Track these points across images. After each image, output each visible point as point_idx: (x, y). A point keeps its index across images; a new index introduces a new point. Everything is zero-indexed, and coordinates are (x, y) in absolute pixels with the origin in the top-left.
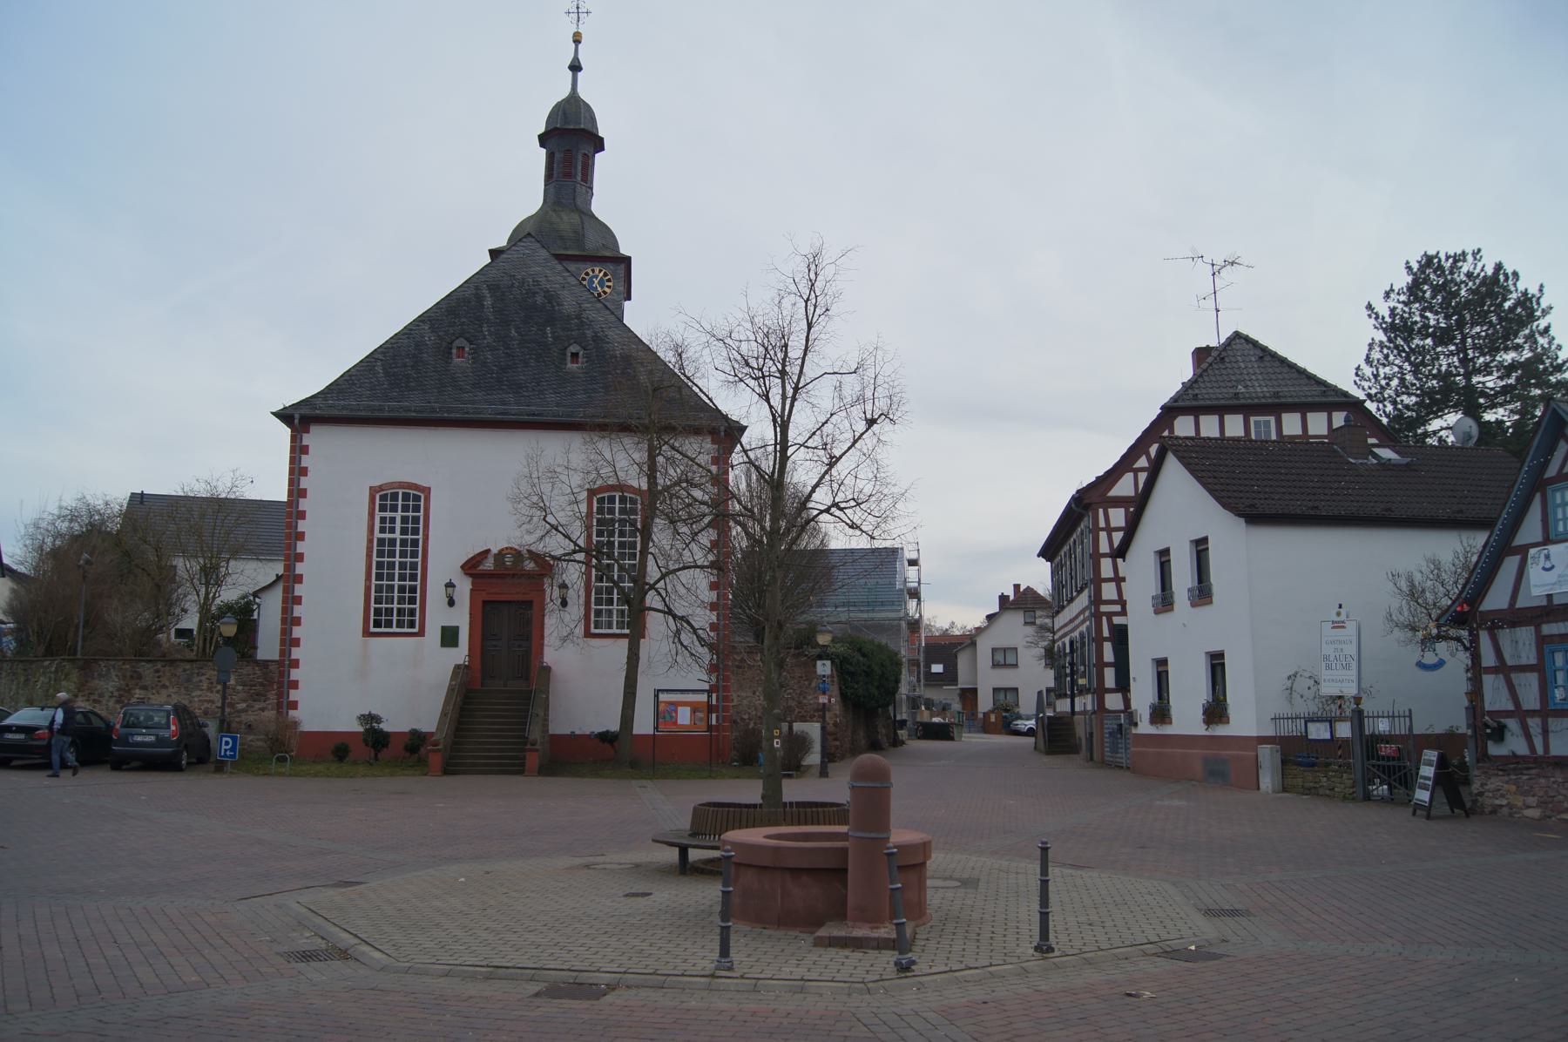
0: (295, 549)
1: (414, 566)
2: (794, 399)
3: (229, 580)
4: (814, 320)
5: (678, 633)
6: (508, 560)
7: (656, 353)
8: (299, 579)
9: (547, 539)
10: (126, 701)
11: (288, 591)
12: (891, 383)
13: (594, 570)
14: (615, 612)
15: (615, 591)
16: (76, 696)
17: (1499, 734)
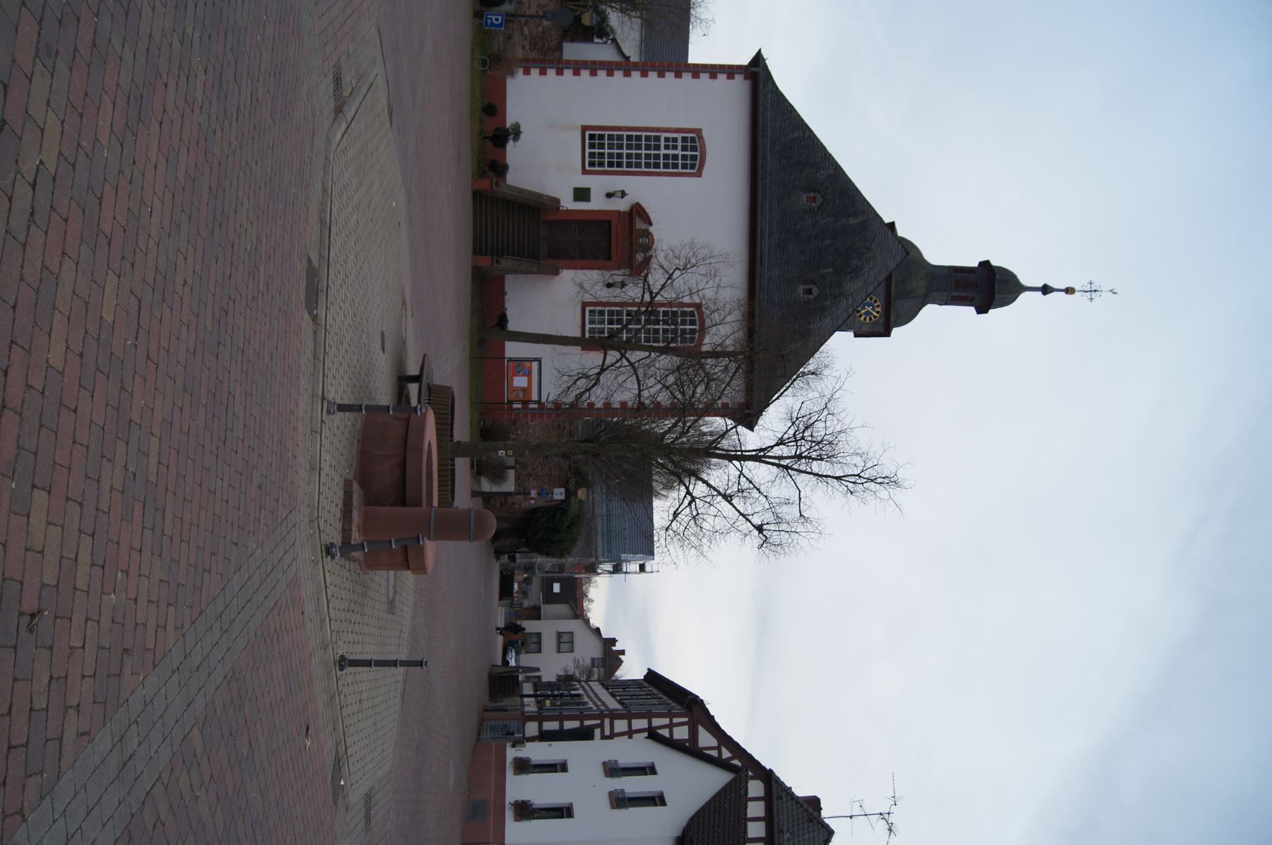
0: (720, 73)
1: (638, 165)
2: (778, 466)
3: (626, 19)
4: (843, 482)
5: (586, 376)
7: (812, 356)
8: (627, 74)
9: (662, 271)
11: (618, 66)
12: (792, 545)
13: (636, 309)
14: (602, 326)
15: (619, 326)
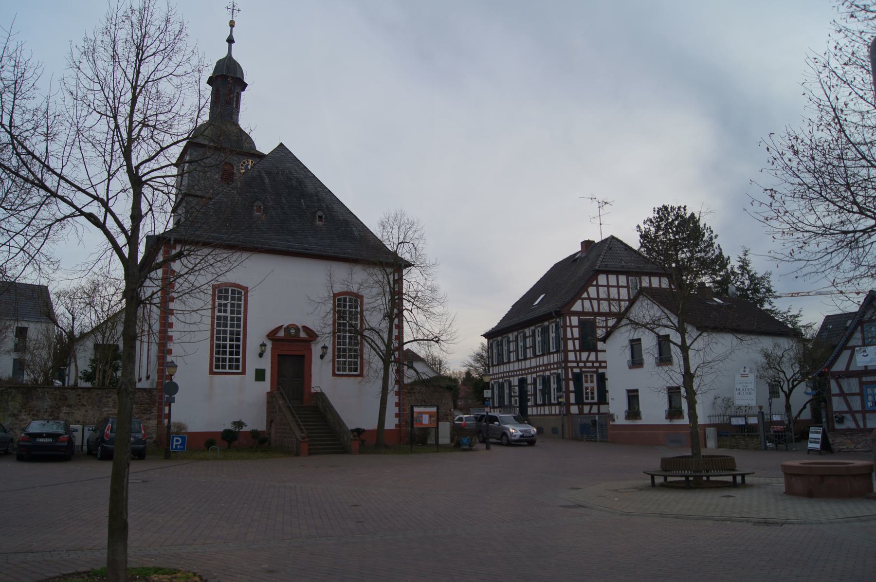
6: (293, 331)
10: (56, 415)
16: (21, 412)
17: (841, 420)
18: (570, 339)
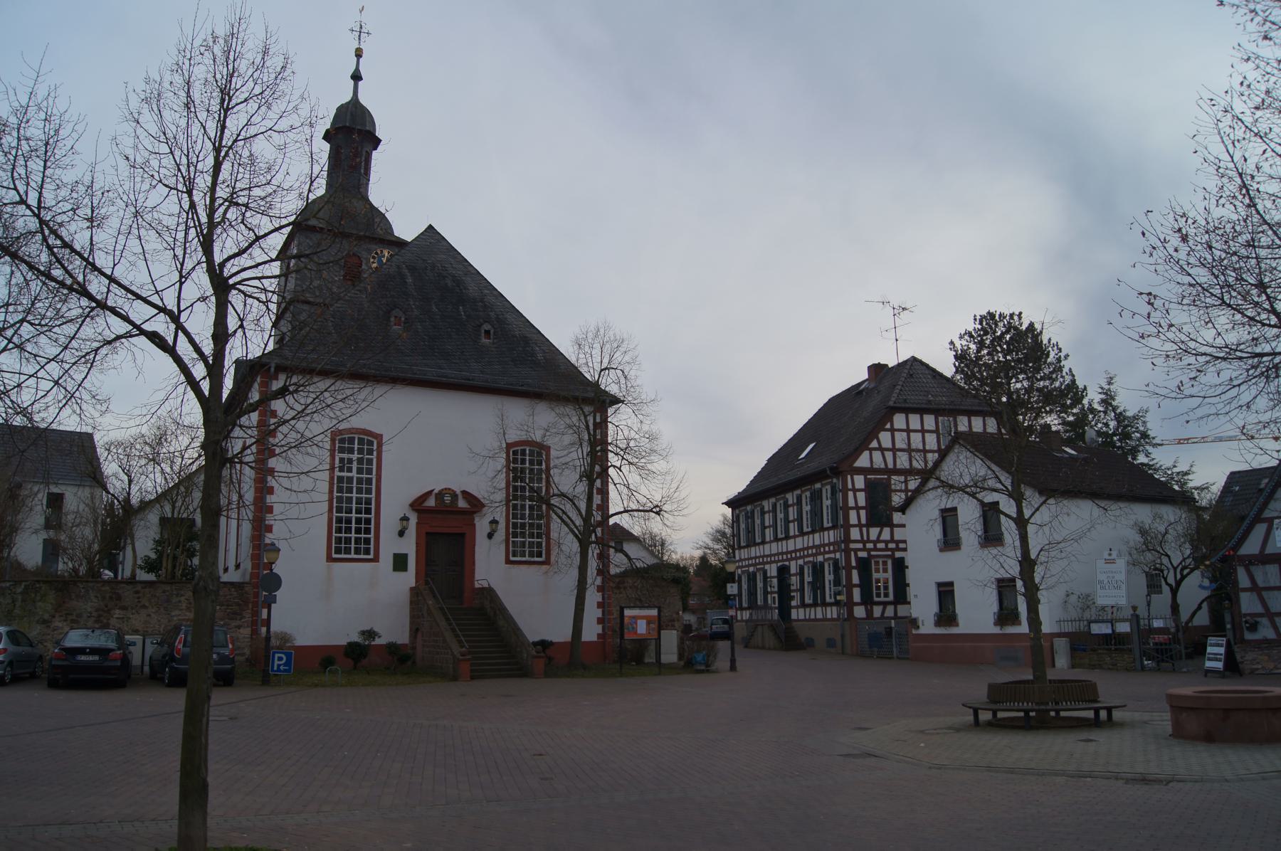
1: (368, 502)
6: (447, 499)
10: (105, 621)
16: (54, 617)
17: (1253, 627)
18: (852, 508)
